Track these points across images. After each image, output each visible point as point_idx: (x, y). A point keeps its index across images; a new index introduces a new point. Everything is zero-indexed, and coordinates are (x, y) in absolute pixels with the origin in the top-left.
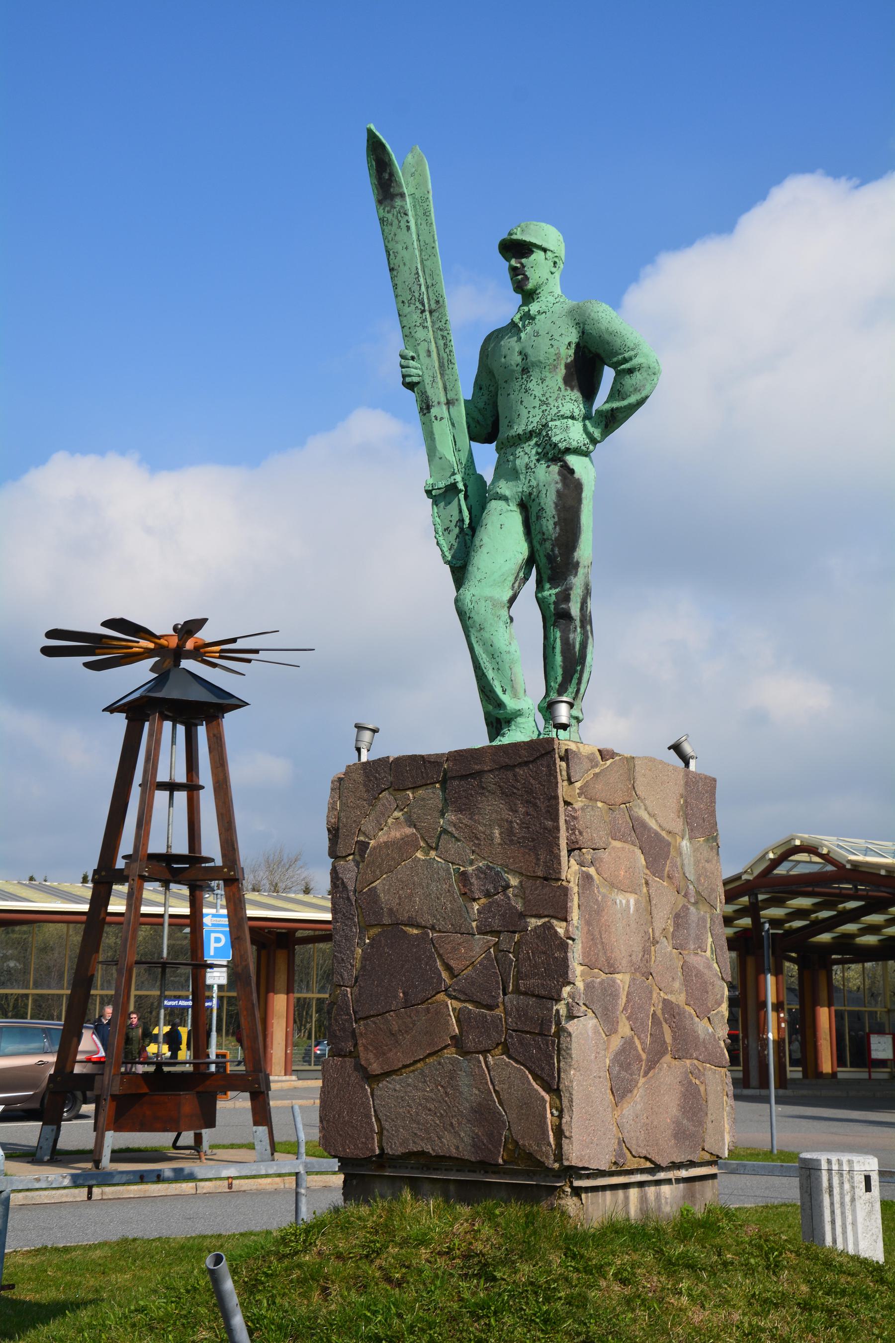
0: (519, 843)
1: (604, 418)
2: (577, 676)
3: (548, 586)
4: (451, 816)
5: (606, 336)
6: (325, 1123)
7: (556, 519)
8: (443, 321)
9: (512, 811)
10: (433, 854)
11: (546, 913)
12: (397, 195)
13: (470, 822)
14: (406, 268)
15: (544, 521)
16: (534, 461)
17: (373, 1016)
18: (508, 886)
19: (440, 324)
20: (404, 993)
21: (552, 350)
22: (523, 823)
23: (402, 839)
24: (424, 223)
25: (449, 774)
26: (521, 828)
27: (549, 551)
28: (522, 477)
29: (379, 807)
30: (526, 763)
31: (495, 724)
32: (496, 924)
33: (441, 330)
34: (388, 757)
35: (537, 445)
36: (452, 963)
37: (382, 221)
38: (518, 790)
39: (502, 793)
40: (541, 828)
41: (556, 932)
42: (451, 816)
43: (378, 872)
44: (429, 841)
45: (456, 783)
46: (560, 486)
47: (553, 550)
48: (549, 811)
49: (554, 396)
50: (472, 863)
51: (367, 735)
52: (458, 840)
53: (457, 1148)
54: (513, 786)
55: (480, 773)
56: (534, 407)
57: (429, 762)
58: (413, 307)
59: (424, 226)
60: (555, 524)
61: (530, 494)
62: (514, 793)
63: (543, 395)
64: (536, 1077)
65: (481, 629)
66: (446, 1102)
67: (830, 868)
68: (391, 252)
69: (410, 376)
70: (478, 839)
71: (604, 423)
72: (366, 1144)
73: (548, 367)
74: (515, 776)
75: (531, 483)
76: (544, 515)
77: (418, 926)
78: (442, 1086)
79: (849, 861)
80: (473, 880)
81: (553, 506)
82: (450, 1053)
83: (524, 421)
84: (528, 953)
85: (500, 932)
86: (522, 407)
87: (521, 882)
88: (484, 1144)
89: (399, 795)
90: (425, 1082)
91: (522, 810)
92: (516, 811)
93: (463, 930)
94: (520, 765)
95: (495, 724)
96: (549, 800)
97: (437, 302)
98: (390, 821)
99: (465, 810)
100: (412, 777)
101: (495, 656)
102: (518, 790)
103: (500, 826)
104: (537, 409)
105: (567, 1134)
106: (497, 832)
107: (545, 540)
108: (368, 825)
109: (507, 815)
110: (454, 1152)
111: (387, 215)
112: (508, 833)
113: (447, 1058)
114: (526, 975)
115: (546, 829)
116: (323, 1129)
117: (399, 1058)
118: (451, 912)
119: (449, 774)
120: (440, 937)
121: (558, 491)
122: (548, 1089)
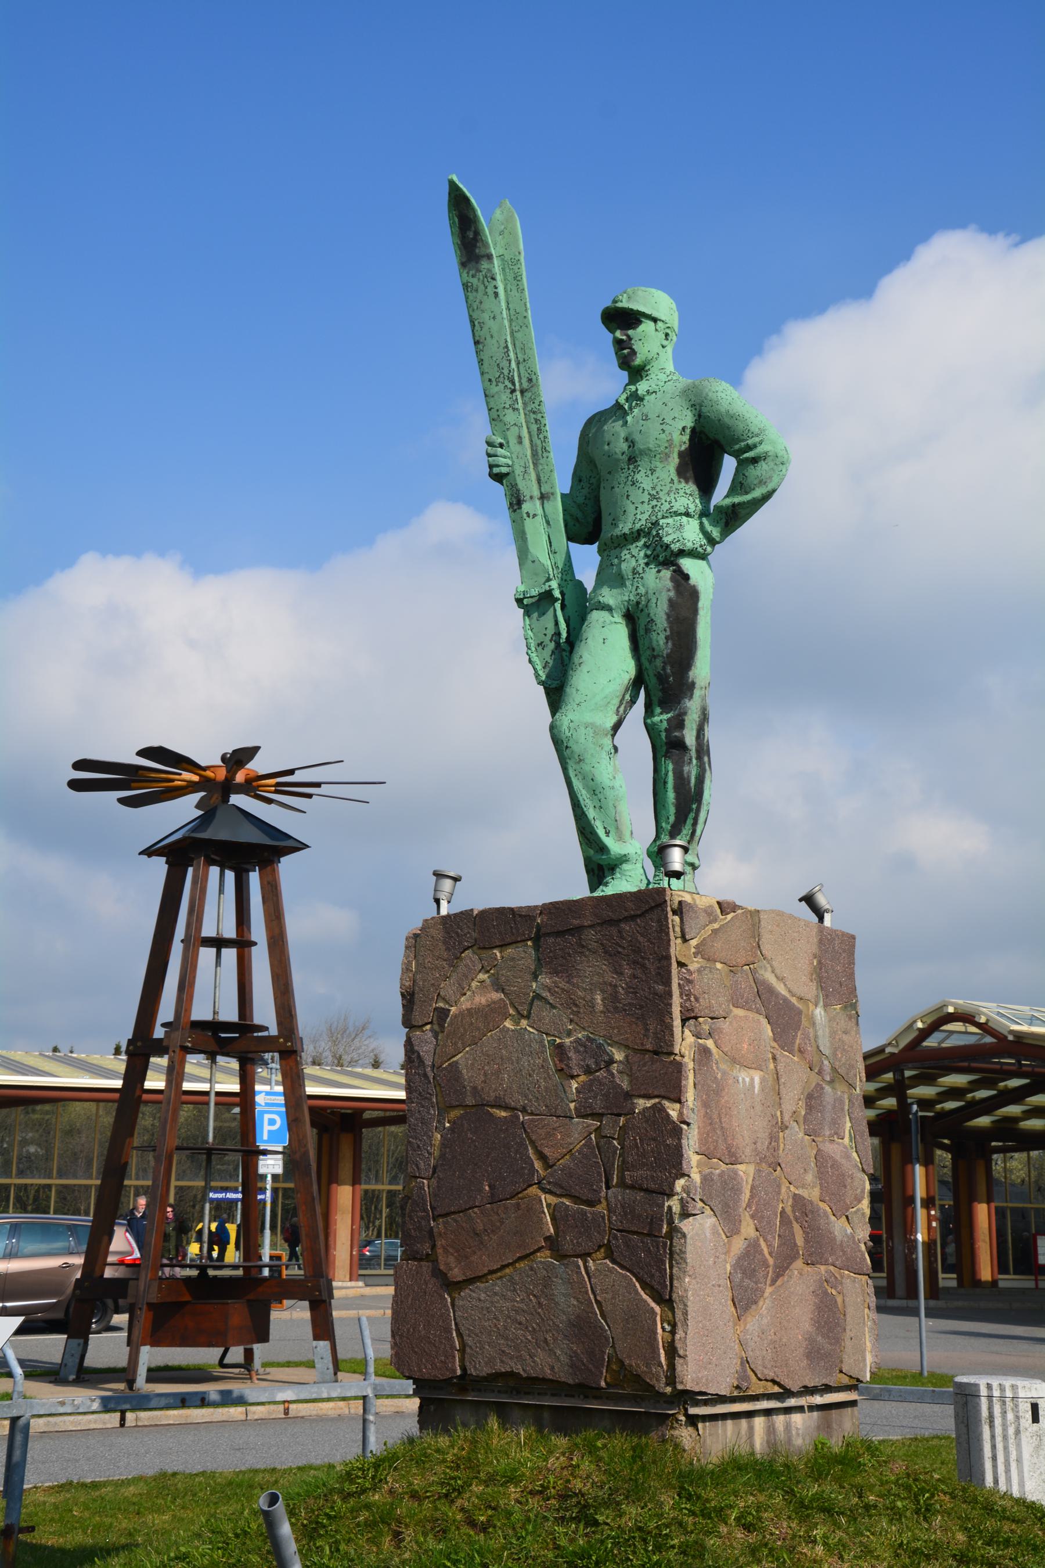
0: (625, 1010)
1: (724, 516)
2: (692, 815)
3: (658, 710)
4: (545, 979)
5: (726, 420)
6: (397, 1338)
7: (668, 633)
8: (537, 402)
9: (617, 973)
10: (524, 1023)
11: (656, 1093)
12: (483, 256)
13: (567, 986)
14: (494, 341)
15: (654, 635)
16: (643, 565)
17: (454, 1213)
18: (612, 1061)
19: (533, 406)
20: (490, 1186)
21: (663, 436)
22: (630, 987)
23: (489, 1005)
24: (514, 288)
25: (543, 930)
26: (627, 993)
27: (659, 670)
28: (628, 583)
29: (462, 968)
30: (633, 918)
31: (596, 872)
32: (598, 1105)
33: (534, 413)
34: (472, 910)
35: (646, 546)
36: (546, 1151)
37: (466, 286)
38: (624, 948)
39: (606, 952)
40: (650, 993)
41: (668, 1115)
42: (545, 979)
43: (460, 1045)
44: (520, 1008)
45: (551, 940)
46: (672, 594)
47: (664, 669)
48: (659, 974)
49: (666, 489)
50: (569, 1034)
51: (447, 884)
52: (553, 1007)
53: (552, 1368)
54: (617, 944)
55: (580, 929)
56: (643, 503)
57: (520, 916)
58: (501, 386)
59: (514, 293)
60: (667, 638)
61: (638, 603)
62: (619, 953)
63: (653, 488)
64: (645, 1286)
65: (580, 760)
66: (539, 1313)
67: (989, 1039)
68: (476, 323)
69: (498, 466)
70: (576, 1005)
71: (724, 520)
72: (445, 1363)
73: (658, 456)
74: (619, 932)
75: (639, 591)
76: (654, 628)
77: (506, 1108)
78: (534, 1296)
79: (1012, 1032)
80: (571, 1054)
81: (665, 617)
82: (544, 1257)
83: (631, 518)
84: (635, 1140)
85: (602, 1115)
86: (628, 502)
87: (627, 1057)
88: (584, 1364)
89: (485, 954)
90: (515, 1290)
91: (628, 972)
92: (622, 974)
93: (559, 1113)
94: (626, 919)
95: (596, 872)
96: (660, 960)
97: (530, 380)
98: (474, 984)
99: (561, 972)
100: (500, 933)
101: (597, 792)
102: (624, 948)
103: (603, 991)
104: (645, 505)
105: (681, 1352)
106: (598, 998)
107: (655, 657)
108: (448, 988)
109: (610, 977)
110: (548, 1373)
111: (471, 280)
112: (612, 999)
113: (541, 1262)
114: (633, 1166)
115: (657, 994)
116: (395, 1345)
117: (484, 1262)
118: (546, 1091)
119: (543, 930)
120: (532, 1120)
121: (670, 600)
122: (659, 1300)
